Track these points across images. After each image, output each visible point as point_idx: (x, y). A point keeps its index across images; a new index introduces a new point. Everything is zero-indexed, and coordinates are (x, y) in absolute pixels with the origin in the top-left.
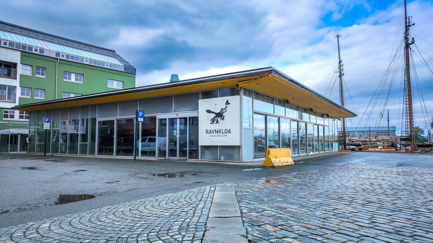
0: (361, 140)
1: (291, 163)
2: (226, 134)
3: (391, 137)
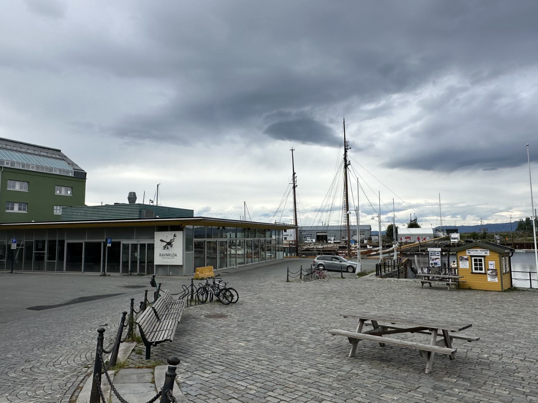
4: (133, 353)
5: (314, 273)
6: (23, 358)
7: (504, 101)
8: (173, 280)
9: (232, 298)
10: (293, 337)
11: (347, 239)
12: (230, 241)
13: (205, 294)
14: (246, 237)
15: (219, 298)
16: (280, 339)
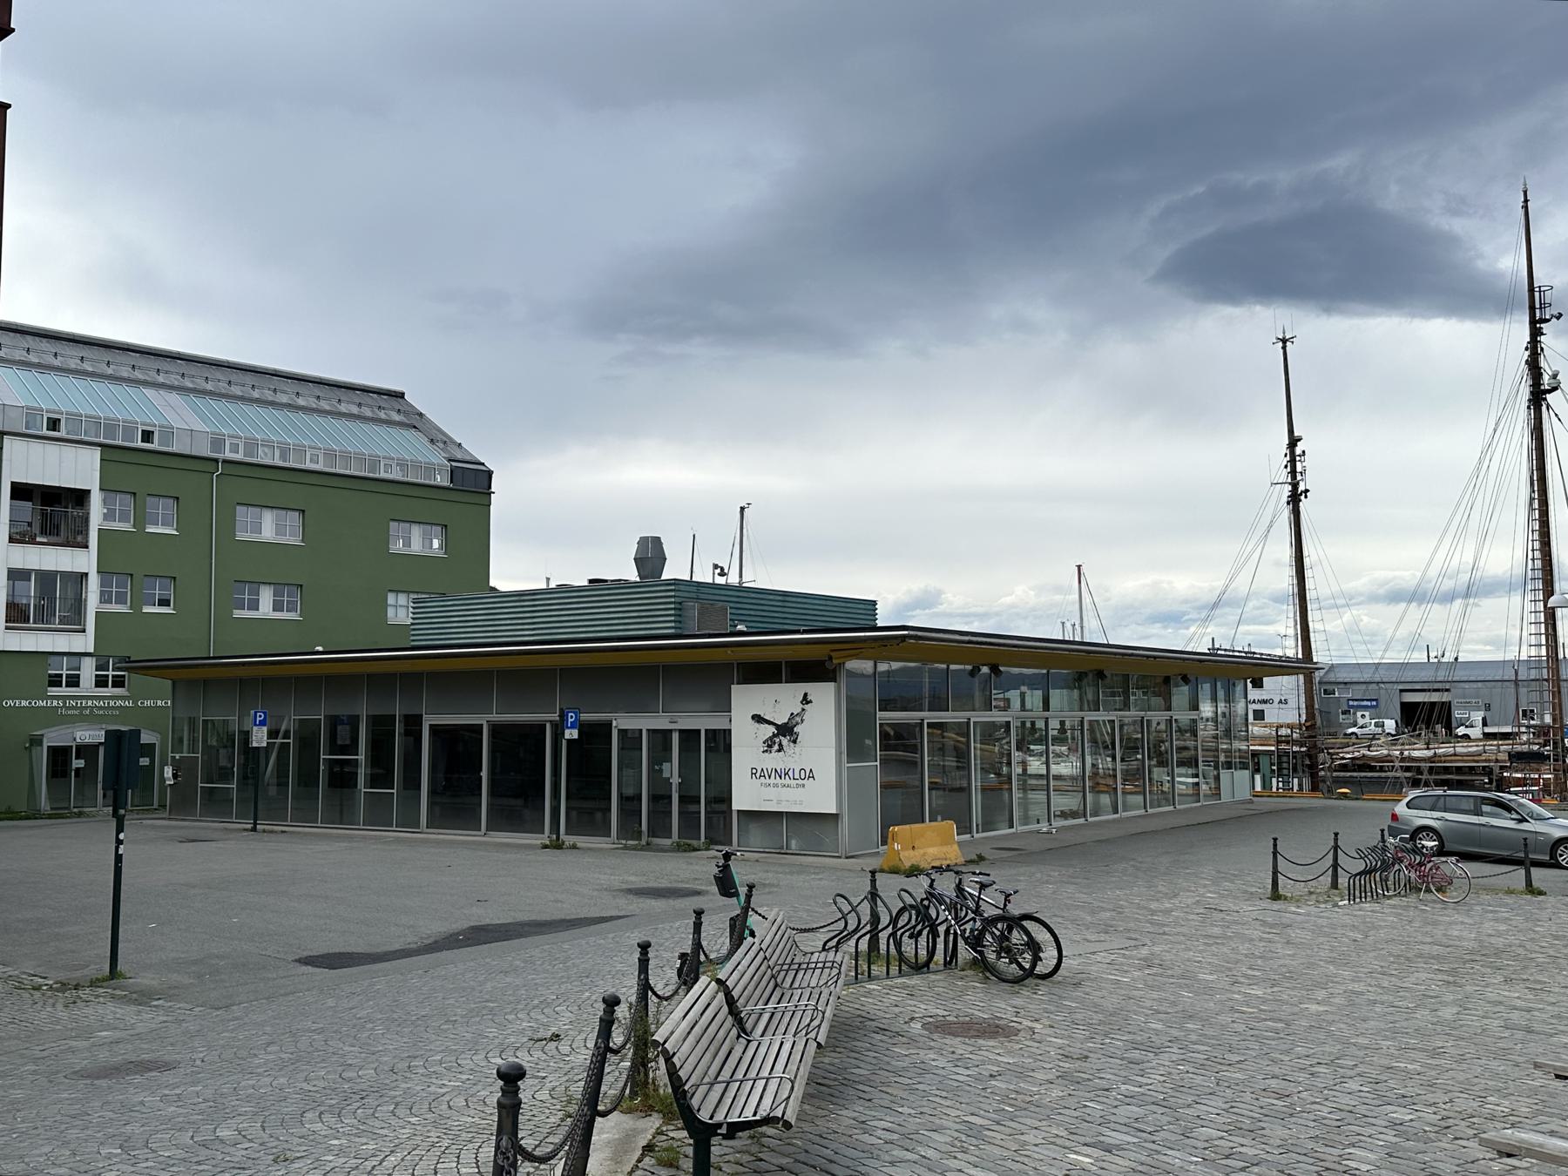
0: (1375, 753)
1: (955, 861)
2: (802, 782)
3: (1484, 746)
4: (647, 1159)
5: (1397, 867)
6: (270, 1145)
8: (803, 869)
9: (1036, 959)
10: (1311, 1145)
11: (1548, 719)
12: (1023, 723)
13: (925, 932)
14: (1086, 707)
15: (982, 953)
16: (1251, 1152)
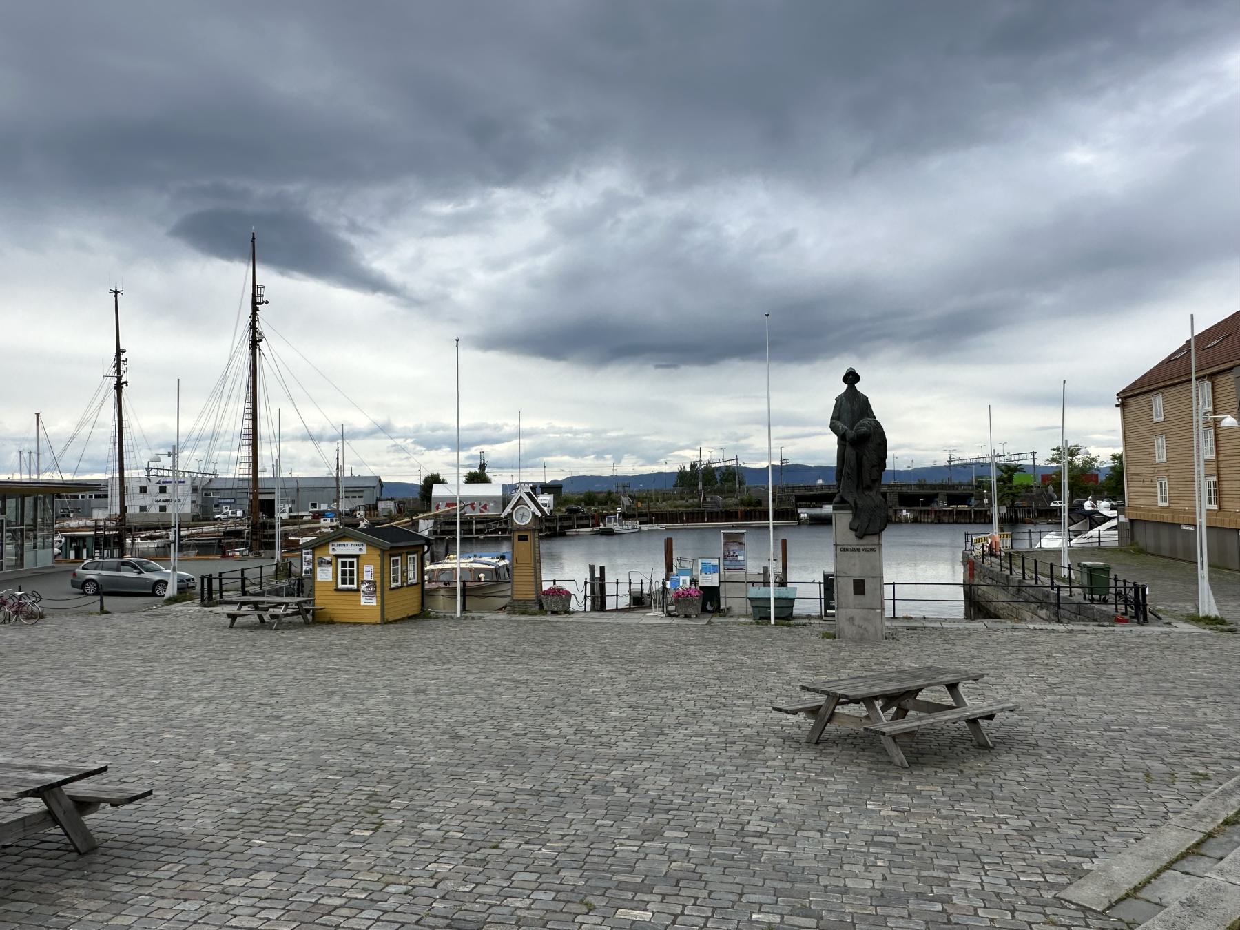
7: (699, 236)
